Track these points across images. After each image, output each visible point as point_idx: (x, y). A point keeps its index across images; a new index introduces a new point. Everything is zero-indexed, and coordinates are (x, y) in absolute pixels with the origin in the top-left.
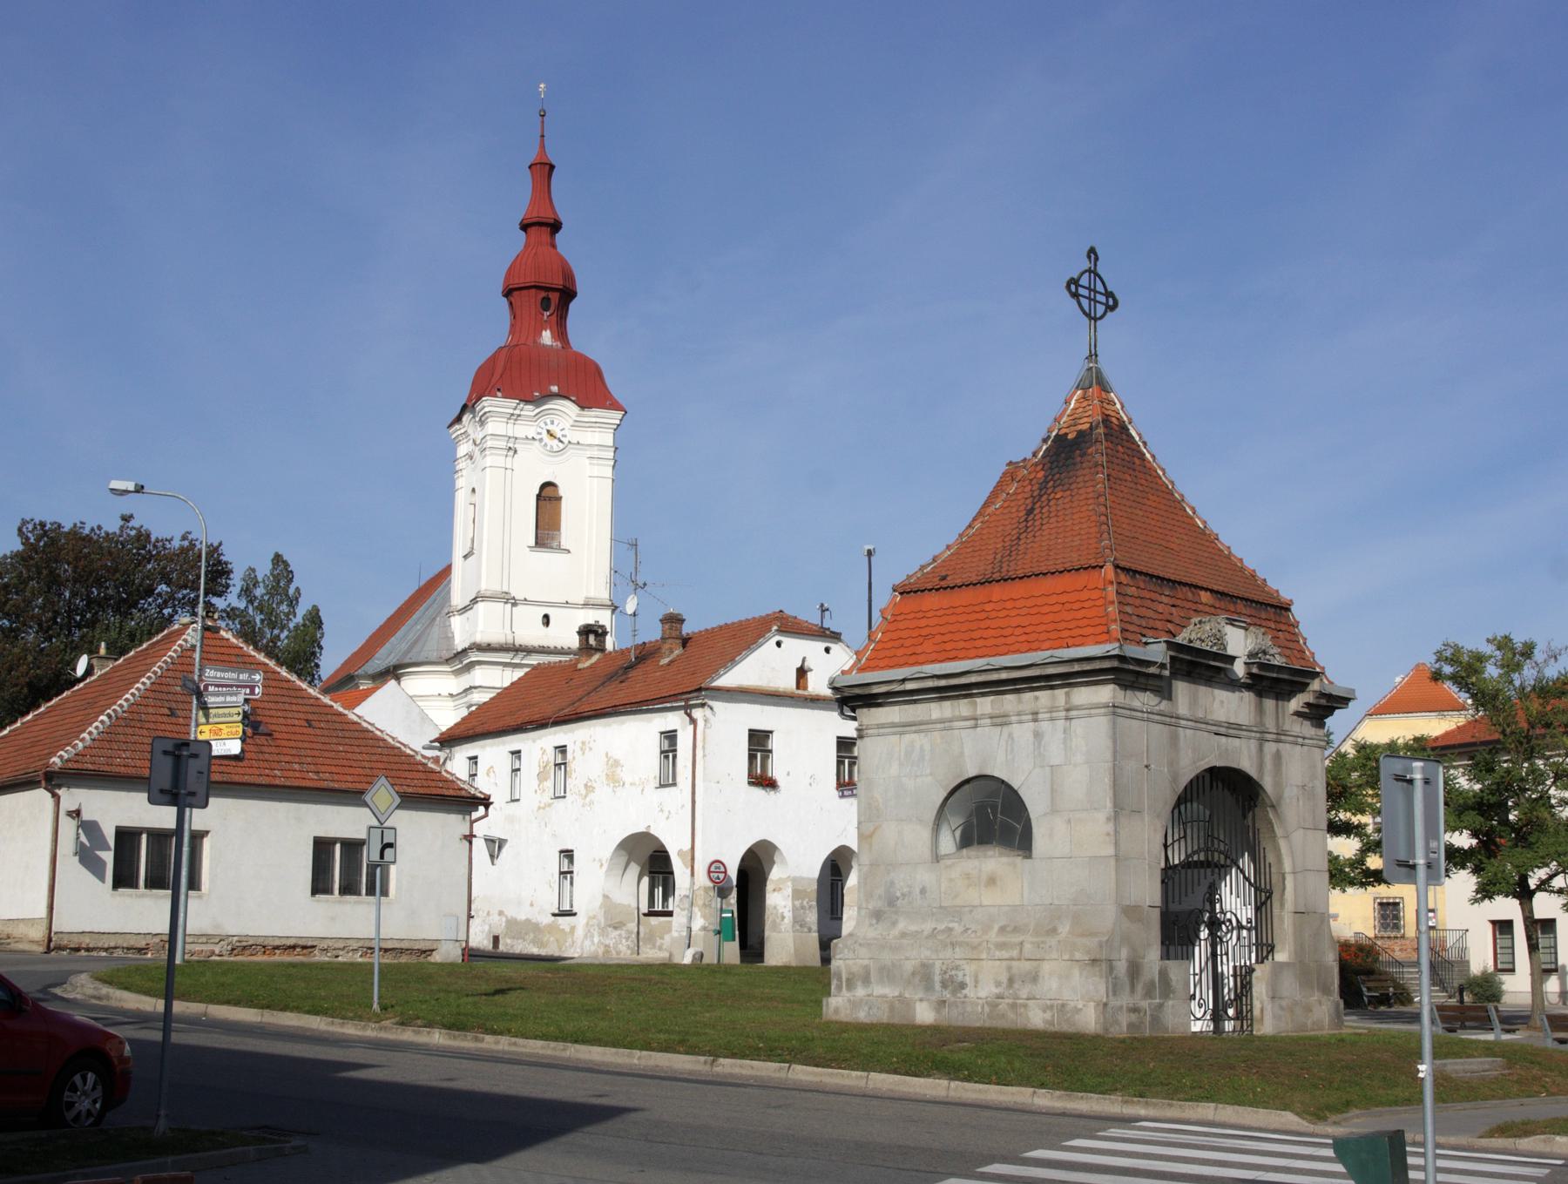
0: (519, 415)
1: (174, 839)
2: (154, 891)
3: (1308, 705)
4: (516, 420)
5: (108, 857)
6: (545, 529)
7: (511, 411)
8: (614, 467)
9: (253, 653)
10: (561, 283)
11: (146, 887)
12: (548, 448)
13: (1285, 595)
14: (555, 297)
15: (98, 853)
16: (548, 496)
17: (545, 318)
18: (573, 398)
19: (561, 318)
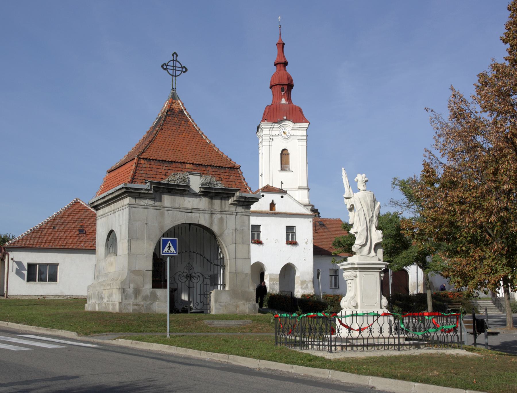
0: (273, 128)
1: (48, 266)
2: (41, 282)
3: (236, 201)
4: (272, 129)
5: (25, 272)
6: (284, 165)
7: (270, 126)
8: (307, 142)
9: (90, 209)
10: (287, 82)
11: (39, 281)
12: (284, 138)
13: (238, 164)
14: (285, 87)
15: (22, 271)
16: (284, 153)
17: (283, 94)
18: (291, 120)
19: (289, 94)
